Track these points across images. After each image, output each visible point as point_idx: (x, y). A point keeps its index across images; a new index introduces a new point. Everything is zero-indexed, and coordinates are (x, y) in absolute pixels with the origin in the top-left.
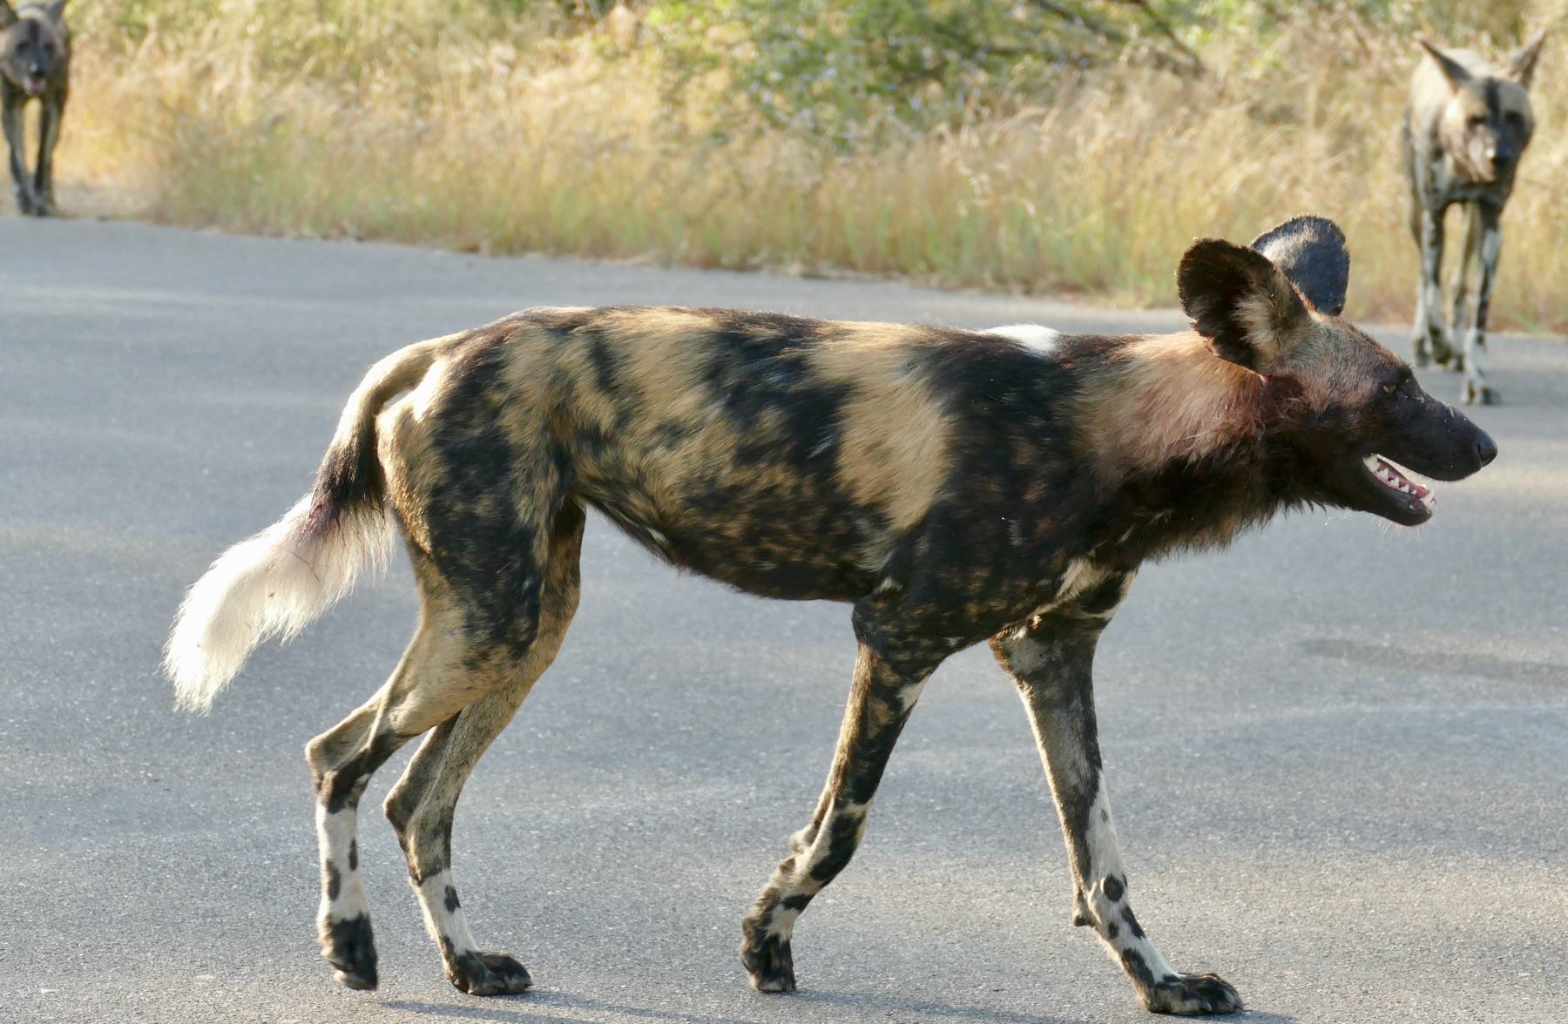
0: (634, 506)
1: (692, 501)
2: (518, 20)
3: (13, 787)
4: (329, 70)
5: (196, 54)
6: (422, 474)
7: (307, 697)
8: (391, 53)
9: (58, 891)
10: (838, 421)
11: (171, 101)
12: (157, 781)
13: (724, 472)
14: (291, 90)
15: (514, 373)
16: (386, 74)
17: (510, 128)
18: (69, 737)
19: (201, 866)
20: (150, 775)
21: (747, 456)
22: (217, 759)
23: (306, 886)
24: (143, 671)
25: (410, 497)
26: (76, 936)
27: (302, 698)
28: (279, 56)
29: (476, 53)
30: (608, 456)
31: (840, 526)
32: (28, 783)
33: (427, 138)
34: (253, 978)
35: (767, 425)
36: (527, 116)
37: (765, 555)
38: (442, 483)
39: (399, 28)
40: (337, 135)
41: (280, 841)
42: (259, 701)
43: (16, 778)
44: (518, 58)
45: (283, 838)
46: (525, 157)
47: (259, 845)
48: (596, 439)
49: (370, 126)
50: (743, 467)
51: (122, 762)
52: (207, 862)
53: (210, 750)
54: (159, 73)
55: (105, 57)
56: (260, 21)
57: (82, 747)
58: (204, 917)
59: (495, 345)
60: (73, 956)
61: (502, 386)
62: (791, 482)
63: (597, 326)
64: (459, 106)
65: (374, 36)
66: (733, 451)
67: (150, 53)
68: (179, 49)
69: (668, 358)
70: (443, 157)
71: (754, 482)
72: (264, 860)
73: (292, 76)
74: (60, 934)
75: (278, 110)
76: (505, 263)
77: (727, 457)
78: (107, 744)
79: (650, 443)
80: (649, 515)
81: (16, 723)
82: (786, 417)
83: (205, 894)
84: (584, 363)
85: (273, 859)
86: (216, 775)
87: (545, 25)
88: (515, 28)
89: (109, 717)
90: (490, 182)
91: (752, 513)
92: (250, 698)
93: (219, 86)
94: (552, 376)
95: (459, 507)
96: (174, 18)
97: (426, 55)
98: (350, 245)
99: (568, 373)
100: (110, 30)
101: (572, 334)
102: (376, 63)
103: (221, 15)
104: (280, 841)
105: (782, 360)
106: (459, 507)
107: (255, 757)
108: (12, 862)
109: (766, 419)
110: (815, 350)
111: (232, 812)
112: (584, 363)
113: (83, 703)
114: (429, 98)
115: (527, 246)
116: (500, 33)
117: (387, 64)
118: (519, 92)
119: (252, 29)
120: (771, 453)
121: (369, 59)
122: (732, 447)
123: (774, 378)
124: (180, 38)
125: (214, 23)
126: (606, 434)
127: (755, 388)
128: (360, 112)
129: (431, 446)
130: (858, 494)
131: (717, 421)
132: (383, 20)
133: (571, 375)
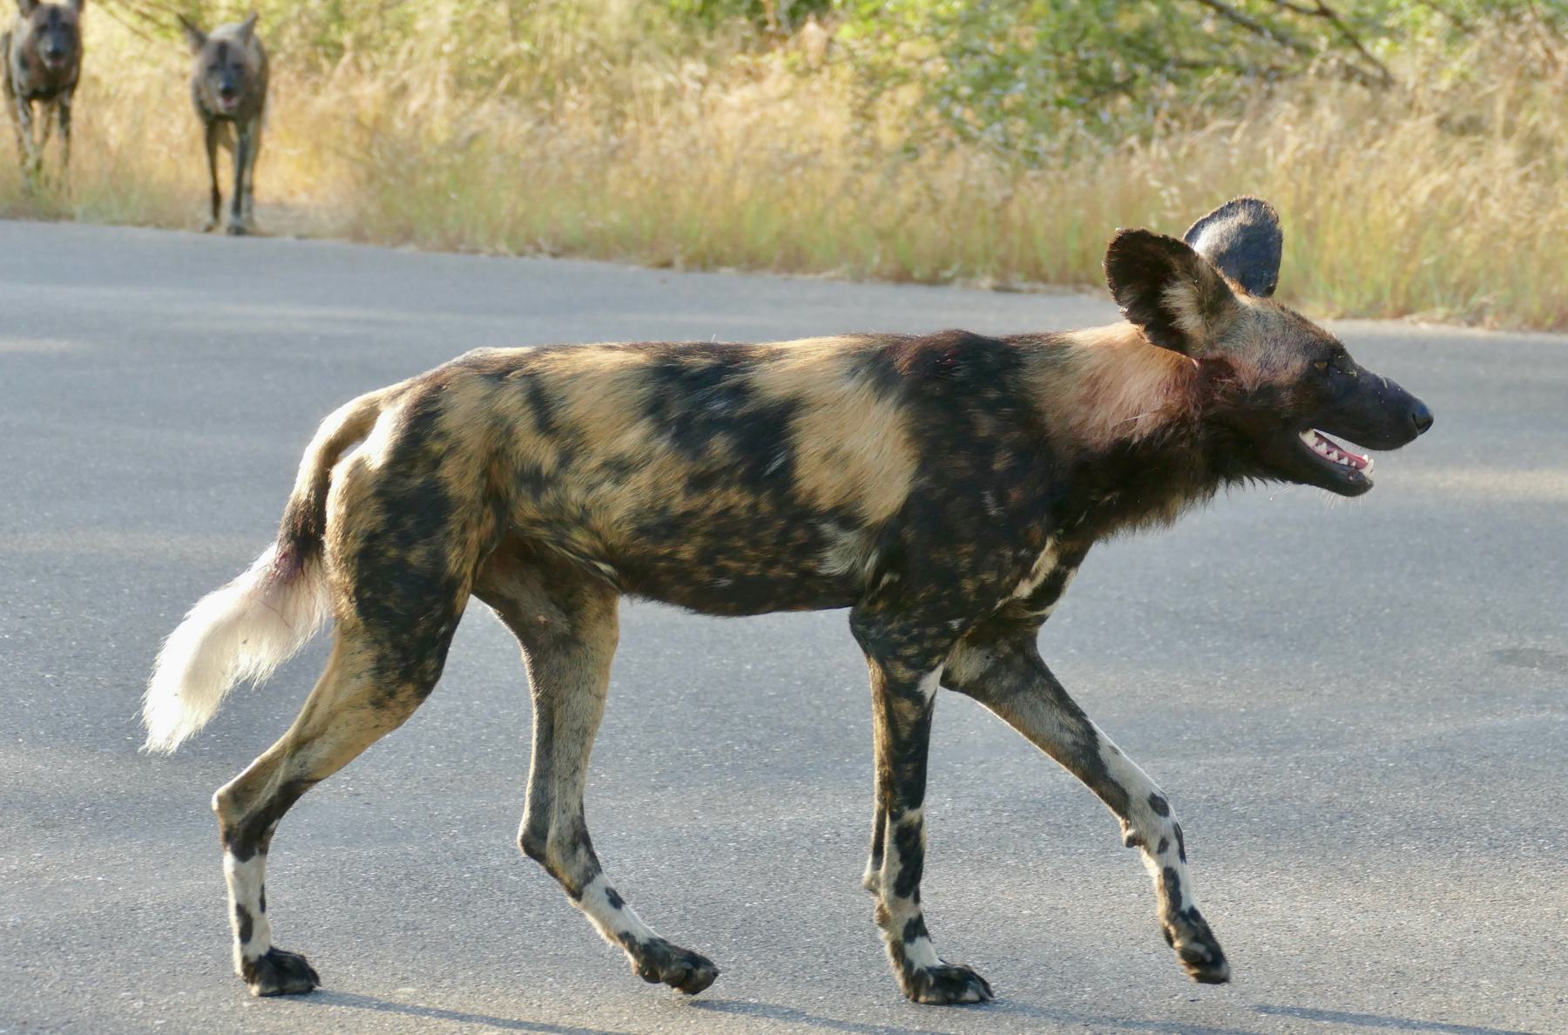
0: (578, 542)
1: (642, 531)
2: (710, 37)
4: (523, 87)
5: (392, 73)
6: (358, 520)
8: (585, 70)
11: (367, 120)
14: (486, 107)
15: (450, 421)
16: (580, 92)
17: (702, 144)
19: (402, 880)
28: (473, 74)
29: (671, 72)
30: (549, 497)
33: (621, 154)
36: (719, 131)
39: (593, 45)
40: (532, 152)
44: (710, 75)
45: (483, 851)
46: (718, 171)
47: (459, 859)
48: (536, 481)
49: (565, 143)
52: (407, 875)
54: (355, 91)
55: (301, 76)
56: (455, 39)
61: (441, 435)
63: (532, 370)
64: (652, 123)
65: (567, 54)
66: (685, 481)
67: (346, 72)
68: (375, 68)
69: (606, 396)
73: (487, 94)
75: (473, 128)
76: (698, 277)
77: (679, 487)
80: (595, 550)
81: (217, 738)
83: (406, 907)
85: (473, 872)
87: (737, 44)
88: (707, 45)
90: (684, 197)
92: (449, 712)
93: (414, 105)
94: (490, 422)
95: (393, 553)
96: (369, 37)
97: (619, 72)
98: (545, 261)
102: (570, 81)
107: (454, 771)
108: (214, 877)
114: (623, 115)
115: (719, 262)
116: (692, 50)
117: (581, 81)
119: (447, 48)
121: (563, 76)
122: (683, 476)
124: (375, 56)
125: (410, 42)
126: (547, 474)
128: (554, 129)
132: (577, 38)
133: (510, 420)
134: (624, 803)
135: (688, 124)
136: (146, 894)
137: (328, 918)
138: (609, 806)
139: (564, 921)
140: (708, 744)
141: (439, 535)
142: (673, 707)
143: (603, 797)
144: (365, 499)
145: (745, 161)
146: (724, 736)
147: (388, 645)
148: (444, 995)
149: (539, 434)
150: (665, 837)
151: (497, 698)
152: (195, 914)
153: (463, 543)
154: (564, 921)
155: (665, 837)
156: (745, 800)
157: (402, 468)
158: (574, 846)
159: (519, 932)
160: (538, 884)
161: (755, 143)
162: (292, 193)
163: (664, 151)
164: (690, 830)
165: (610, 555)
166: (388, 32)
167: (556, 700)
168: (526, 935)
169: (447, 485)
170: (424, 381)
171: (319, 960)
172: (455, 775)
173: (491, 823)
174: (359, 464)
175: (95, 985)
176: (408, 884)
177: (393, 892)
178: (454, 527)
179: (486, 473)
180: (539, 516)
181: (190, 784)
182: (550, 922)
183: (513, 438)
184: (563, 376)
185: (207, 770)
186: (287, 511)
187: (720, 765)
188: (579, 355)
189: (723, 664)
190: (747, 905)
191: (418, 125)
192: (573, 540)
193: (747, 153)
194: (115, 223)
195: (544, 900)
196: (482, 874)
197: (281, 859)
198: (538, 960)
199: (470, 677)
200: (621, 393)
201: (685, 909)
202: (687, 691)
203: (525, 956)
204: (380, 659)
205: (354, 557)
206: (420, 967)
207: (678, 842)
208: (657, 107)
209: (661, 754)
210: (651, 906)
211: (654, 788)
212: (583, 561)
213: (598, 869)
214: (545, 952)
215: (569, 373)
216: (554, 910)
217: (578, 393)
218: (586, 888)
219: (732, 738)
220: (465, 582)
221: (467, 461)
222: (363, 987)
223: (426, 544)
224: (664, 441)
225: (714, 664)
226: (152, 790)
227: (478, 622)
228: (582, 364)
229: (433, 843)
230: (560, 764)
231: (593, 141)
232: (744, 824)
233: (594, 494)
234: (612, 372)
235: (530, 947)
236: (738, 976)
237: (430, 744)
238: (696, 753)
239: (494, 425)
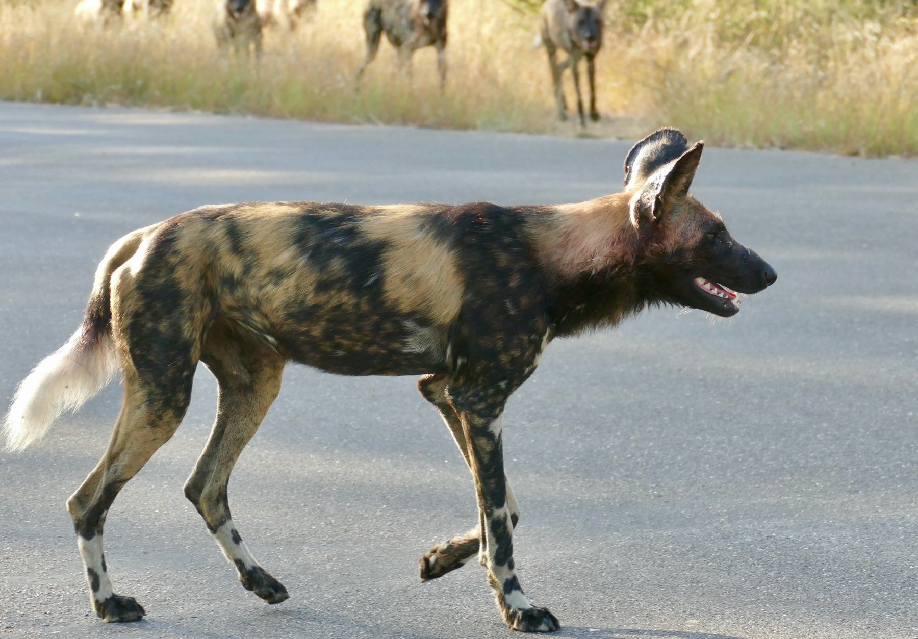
0: (255, 321)
1: (290, 315)
2: (882, 6)
3: (569, 501)
4: (762, 40)
5: (678, 33)
6: (128, 305)
7: (754, 443)
8: (802, 29)
9: (599, 566)
10: (381, 263)
11: (662, 63)
12: (660, 496)
13: (309, 297)
14: (738, 54)
15: (182, 244)
16: (799, 43)
17: (878, 75)
18: (604, 469)
19: (689, 551)
20: (655, 492)
21: (322, 287)
22: (698, 482)
23: (756, 563)
24: (650, 426)
25: (121, 318)
26: (610, 595)
27: (751, 443)
28: (730, 33)
29: (856, 29)
30: (239, 293)
31: (388, 326)
32: (579, 498)
33: (826, 83)
34: (723, 622)
35: (334, 268)
36: (889, 68)
37: (338, 346)
38: (141, 311)
39: (806, 13)
40: (768, 82)
41: (738, 534)
42: (724, 445)
43: (571, 495)
44: (882, 31)
45: (740, 533)
46: (887, 93)
47: (725, 537)
48: (231, 283)
49: (790, 75)
50: (320, 294)
51: (638, 484)
52: (693, 548)
53: (693, 476)
54: (655, 45)
55: (620, 36)
56: (718, 10)
57: (612, 475)
58: (691, 582)
59: (173, 228)
60: (609, 608)
61: (176, 253)
62: (353, 301)
63: (231, 215)
64: (845, 63)
65: (790, 18)
66: (314, 284)
67: (649, 32)
68: (667, 30)
69: (272, 232)
70: (835, 95)
71: (328, 302)
72: (729, 546)
73: (739, 45)
74: (601, 594)
75: (730, 67)
76: (876, 162)
77: (311, 288)
78: (628, 473)
79: (264, 283)
80: (264, 326)
81: (570, 460)
82: (347, 263)
83: (692, 568)
84: (223, 237)
85: (734, 546)
86: (697, 492)
87: (900, 12)
88: (880, 12)
89: (629, 456)
90: (866, 109)
91: (328, 320)
92: (718, 443)
93: (692, 52)
94: (205, 246)
95: (149, 325)
96: (663, 9)
97: (823, 30)
98: (777, 153)
99: (214, 243)
100: (623, 19)
101: (216, 221)
102: (792, 36)
103: (694, 8)
104: (738, 534)
105: (343, 229)
106: (149, 325)
107: (722, 481)
108: (569, 548)
109: (333, 265)
110: (362, 222)
111: (707, 516)
112: (223, 237)
113: (612, 447)
114: (826, 58)
115: (889, 152)
116: (871, 15)
117: (799, 36)
118: (880, 54)
119: (713, 16)
120: (338, 285)
121: (788, 33)
122: (313, 282)
123: (337, 240)
124: (667, 21)
125: (689, 13)
126: (237, 279)
127: (327, 246)
128: (782, 67)
129: (135, 289)
130: (401, 307)
131: (304, 266)
132: (796, 8)
133: (216, 244)
134: (831, 502)
135: (868, 62)
136: (526, 559)
137: (642, 575)
138: (822, 503)
139: (793, 577)
140: (885, 463)
141: (176, 314)
142: (862, 440)
143: (817, 498)
144: (131, 292)
145: (906, 87)
146: (895, 458)
147: (153, 384)
148: (717, 625)
149: (233, 254)
150: (858, 523)
151: (748, 434)
152: (558, 573)
153: (192, 319)
154: (793, 577)
155: (858, 523)
156: (909, 500)
157: (152, 272)
158: (218, 501)
159: (764, 585)
160: (776, 553)
161: (912, 75)
162: (614, 110)
163: (853, 81)
164: (874, 519)
165: (272, 330)
166: (676, 6)
167: (231, 419)
168: (769, 586)
169: (179, 283)
170: (169, 221)
171: (637, 602)
172: (722, 484)
173: (746, 514)
174: (127, 271)
175: (495, 617)
176: (693, 553)
177: (684, 559)
178: (185, 308)
179: (203, 277)
180: (234, 305)
181: (554, 489)
182: (784, 578)
183: (218, 256)
184: (249, 219)
185: (564, 481)
186: (90, 301)
187: (893, 477)
188: (261, 207)
189: (894, 412)
190: (911, 567)
191: (694, 67)
192: (253, 320)
193: (906, 81)
194: (502, 131)
195: (780, 564)
196: (740, 547)
197: (612, 537)
198: (777, 602)
199: (731, 420)
200: (282, 230)
201: (871, 570)
202: (871, 429)
203: (769, 600)
204: (150, 394)
205: (127, 329)
206: (701, 607)
207: (866, 527)
208: (848, 53)
209: (855, 470)
210: (849, 568)
211: (850, 492)
212: (258, 333)
213: (229, 516)
214: (781, 598)
215: (253, 217)
216: (786, 570)
217: (257, 229)
218: (220, 528)
219: (901, 460)
220: (195, 343)
221: (192, 268)
222: (665, 619)
223: (168, 319)
224: (304, 259)
225: (888, 412)
226: (529, 493)
227: (736, 385)
228: (262, 212)
229: (708, 527)
230: (222, 453)
231: (807, 74)
232: (908, 515)
233: (263, 291)
234: (278, 218)
235: (771, 595)
236: (906, 613)
237: (706, 464)
238: (877, 469)
239: (207, 247)
